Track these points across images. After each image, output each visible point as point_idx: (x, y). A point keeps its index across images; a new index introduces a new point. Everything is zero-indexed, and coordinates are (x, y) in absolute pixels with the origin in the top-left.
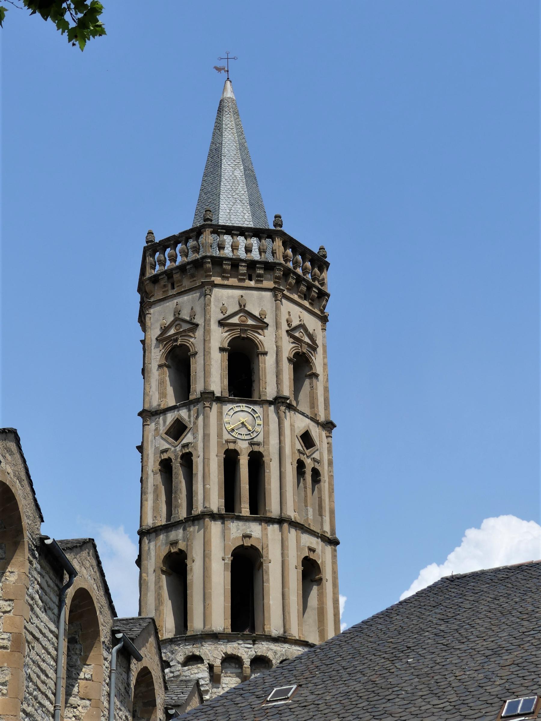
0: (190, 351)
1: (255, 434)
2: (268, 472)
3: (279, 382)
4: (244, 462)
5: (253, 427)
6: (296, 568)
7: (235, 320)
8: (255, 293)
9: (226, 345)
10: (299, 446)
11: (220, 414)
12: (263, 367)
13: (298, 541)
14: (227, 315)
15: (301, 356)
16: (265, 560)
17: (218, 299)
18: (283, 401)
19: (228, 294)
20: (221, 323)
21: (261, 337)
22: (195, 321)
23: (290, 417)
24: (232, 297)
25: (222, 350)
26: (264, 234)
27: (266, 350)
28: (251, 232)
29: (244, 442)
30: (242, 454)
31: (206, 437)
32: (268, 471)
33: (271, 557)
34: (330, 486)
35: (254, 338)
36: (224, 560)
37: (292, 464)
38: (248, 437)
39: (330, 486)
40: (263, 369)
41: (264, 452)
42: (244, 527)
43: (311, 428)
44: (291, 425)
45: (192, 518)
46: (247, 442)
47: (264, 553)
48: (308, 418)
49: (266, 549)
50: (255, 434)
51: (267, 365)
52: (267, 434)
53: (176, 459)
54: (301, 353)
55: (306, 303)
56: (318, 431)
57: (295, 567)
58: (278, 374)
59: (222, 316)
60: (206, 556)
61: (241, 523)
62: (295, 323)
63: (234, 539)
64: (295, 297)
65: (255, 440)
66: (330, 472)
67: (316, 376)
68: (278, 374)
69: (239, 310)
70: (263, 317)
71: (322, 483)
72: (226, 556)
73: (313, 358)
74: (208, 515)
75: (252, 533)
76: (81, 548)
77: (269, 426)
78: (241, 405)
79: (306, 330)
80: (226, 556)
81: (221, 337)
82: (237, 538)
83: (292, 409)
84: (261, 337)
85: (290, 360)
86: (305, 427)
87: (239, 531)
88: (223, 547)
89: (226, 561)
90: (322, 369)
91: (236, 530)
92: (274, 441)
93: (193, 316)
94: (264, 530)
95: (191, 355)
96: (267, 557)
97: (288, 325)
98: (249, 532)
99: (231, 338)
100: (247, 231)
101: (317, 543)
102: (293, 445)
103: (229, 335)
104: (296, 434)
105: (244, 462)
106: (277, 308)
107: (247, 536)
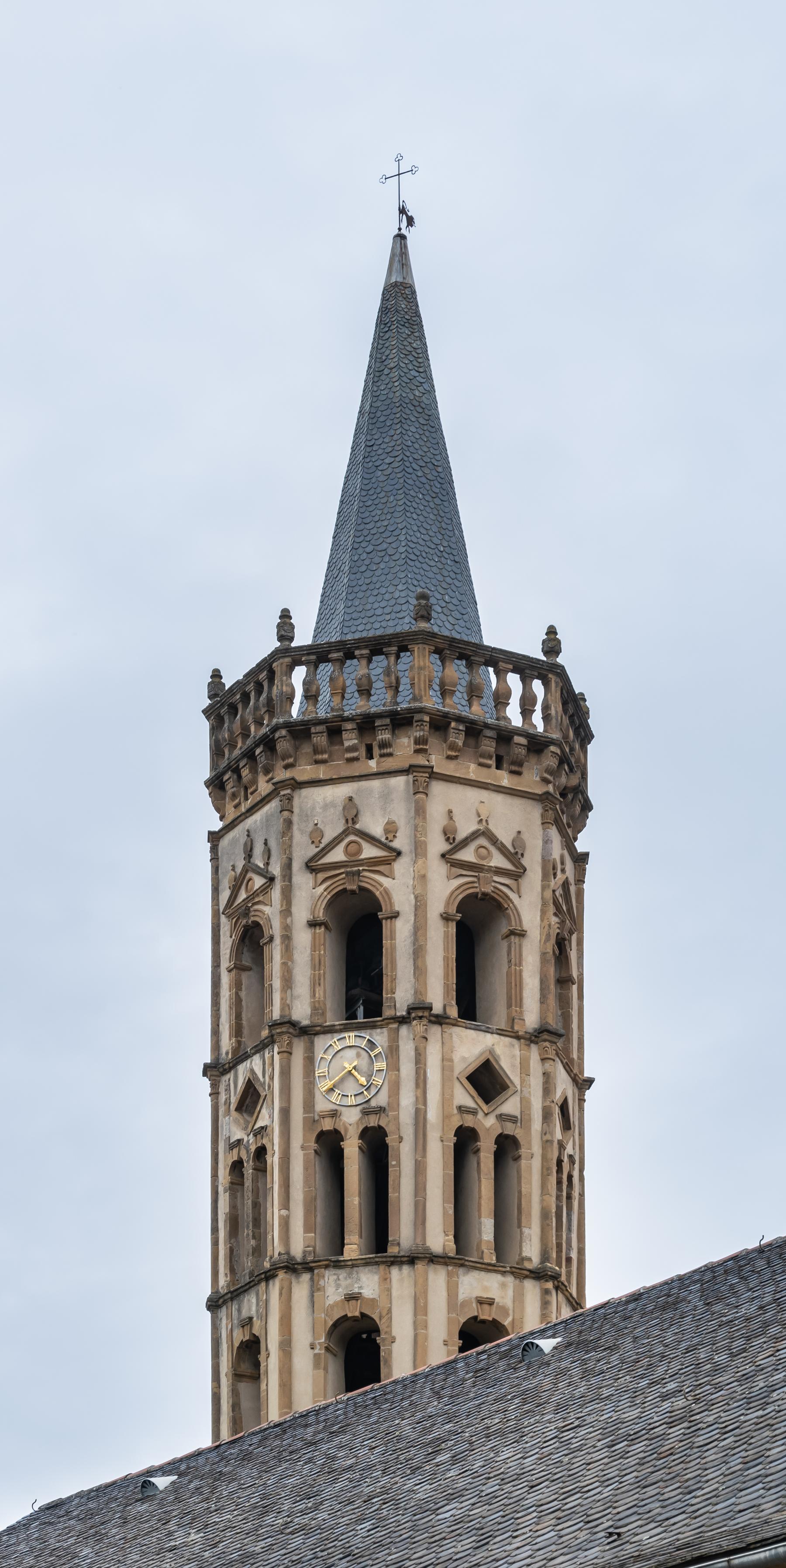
0: (381, 910)
1: (373, 1091)
2: (394, 1166)
3: (420, 972)
4: (352, 1149)
5: (369, 1077)
6: (445, 1345)
7: (338, 855)
8: (376, 784)
9: (321, 915)
10: (464, 1096)
11: (310, 1061)
12: (389, 946)
13: (452, 1291)
14: (322, 846)
15: (481, 899)
16: (384, 1340)
17: (307, 816)
18: (420, 1014)
19: (324, 799)
20: (312, 866)
21: (385, 881)
22: (396, 844)
23: (443, 1043)
24: (333, 804)
25: (313, 924)
26: (390, 646)
27: (397, 909)
28: (366, 647)
29: (353, 1109)
30: (348, 1137)
31: (286, 1113)
32: (394, 1163)
33: (395, 1331)
34: (545, 1164)
35: (374, 886)
36: (312, 1348)
37: (442, 1141)
38: (360, 1100)
39: (545, 1164)
40: (389, 951)
41: (387, 1125)
42: (349, 1281)
43: (499, 1051)
44: (443, 1060)
45: (263, 1276)
46: (359, 1108)
47: (382, 1326)
48: (492, 1033)
49: (386, 1317)
50: (373, 1091)
51: (398, 941)
52: (395, 1089)
53: (248, 1162)
54: (479, 896)
55: (505, 779)
56: (517, 1053)
57: (442, 1343)
58: (418, 952)
59: (313, 850)
60: (286, 1346)
61: (342, 1274)
62: (465, 829)
63: (332, 1307)
64: (472, 771)
65: (373, 1103)
66: (545, 1134)
67: (522, 934)
68: (418, 952)
69: (344, 832)
70: (390, 836)
71: (523, 1162)
72: (317, 1342)
73: (513, 896)
74: (282, 1268)
75: (362, 1291)
76: (319, 1290)
77: (398, 1070)
78: (346, 1035)
79: (494, 840)
80: (317, 1342)
81: (312, 897)
82: (336, 1304)
83: (447, 1024)
84: (385, 881)
85: (446, 918)
86: (482, 1054)
87: (340, 1290)
88: (311, 1326)
89: (317, 1351)
90: (539, 914)
91: (334, 1289)
92: (407, 1099)
93: (391, 829)
94: (386, 1280)
95: (264, 944)
96: (389, 1333)
97: (448, 839)
98: (356, 1290)
99: (329, 897)
100: (358, 648)
101: (503, 1285)
102: (446, 1099)
103: (325, 890)
104: (456, 1073)
105: (352, 1149)
106: (420, 811)
107: (352, 1298)
